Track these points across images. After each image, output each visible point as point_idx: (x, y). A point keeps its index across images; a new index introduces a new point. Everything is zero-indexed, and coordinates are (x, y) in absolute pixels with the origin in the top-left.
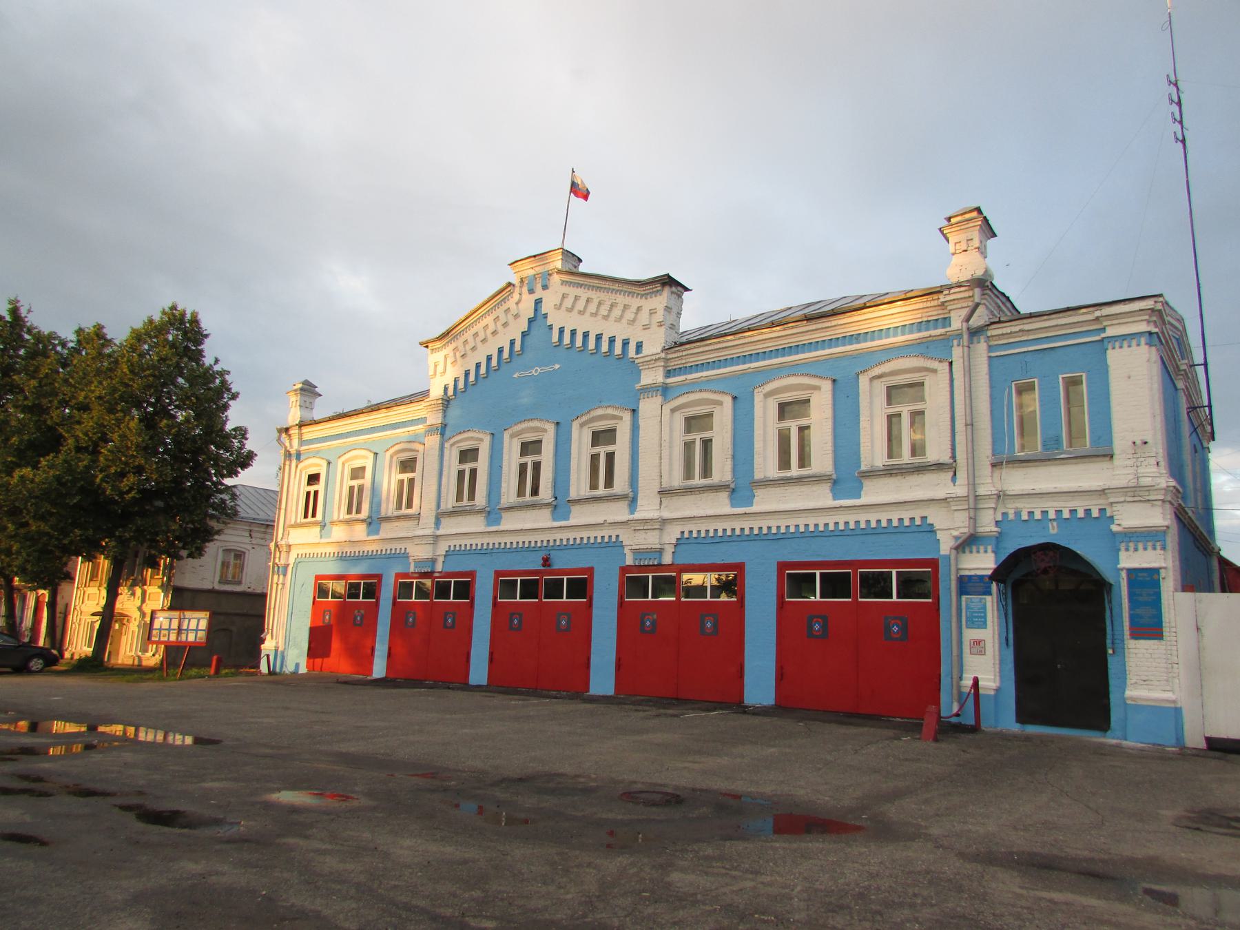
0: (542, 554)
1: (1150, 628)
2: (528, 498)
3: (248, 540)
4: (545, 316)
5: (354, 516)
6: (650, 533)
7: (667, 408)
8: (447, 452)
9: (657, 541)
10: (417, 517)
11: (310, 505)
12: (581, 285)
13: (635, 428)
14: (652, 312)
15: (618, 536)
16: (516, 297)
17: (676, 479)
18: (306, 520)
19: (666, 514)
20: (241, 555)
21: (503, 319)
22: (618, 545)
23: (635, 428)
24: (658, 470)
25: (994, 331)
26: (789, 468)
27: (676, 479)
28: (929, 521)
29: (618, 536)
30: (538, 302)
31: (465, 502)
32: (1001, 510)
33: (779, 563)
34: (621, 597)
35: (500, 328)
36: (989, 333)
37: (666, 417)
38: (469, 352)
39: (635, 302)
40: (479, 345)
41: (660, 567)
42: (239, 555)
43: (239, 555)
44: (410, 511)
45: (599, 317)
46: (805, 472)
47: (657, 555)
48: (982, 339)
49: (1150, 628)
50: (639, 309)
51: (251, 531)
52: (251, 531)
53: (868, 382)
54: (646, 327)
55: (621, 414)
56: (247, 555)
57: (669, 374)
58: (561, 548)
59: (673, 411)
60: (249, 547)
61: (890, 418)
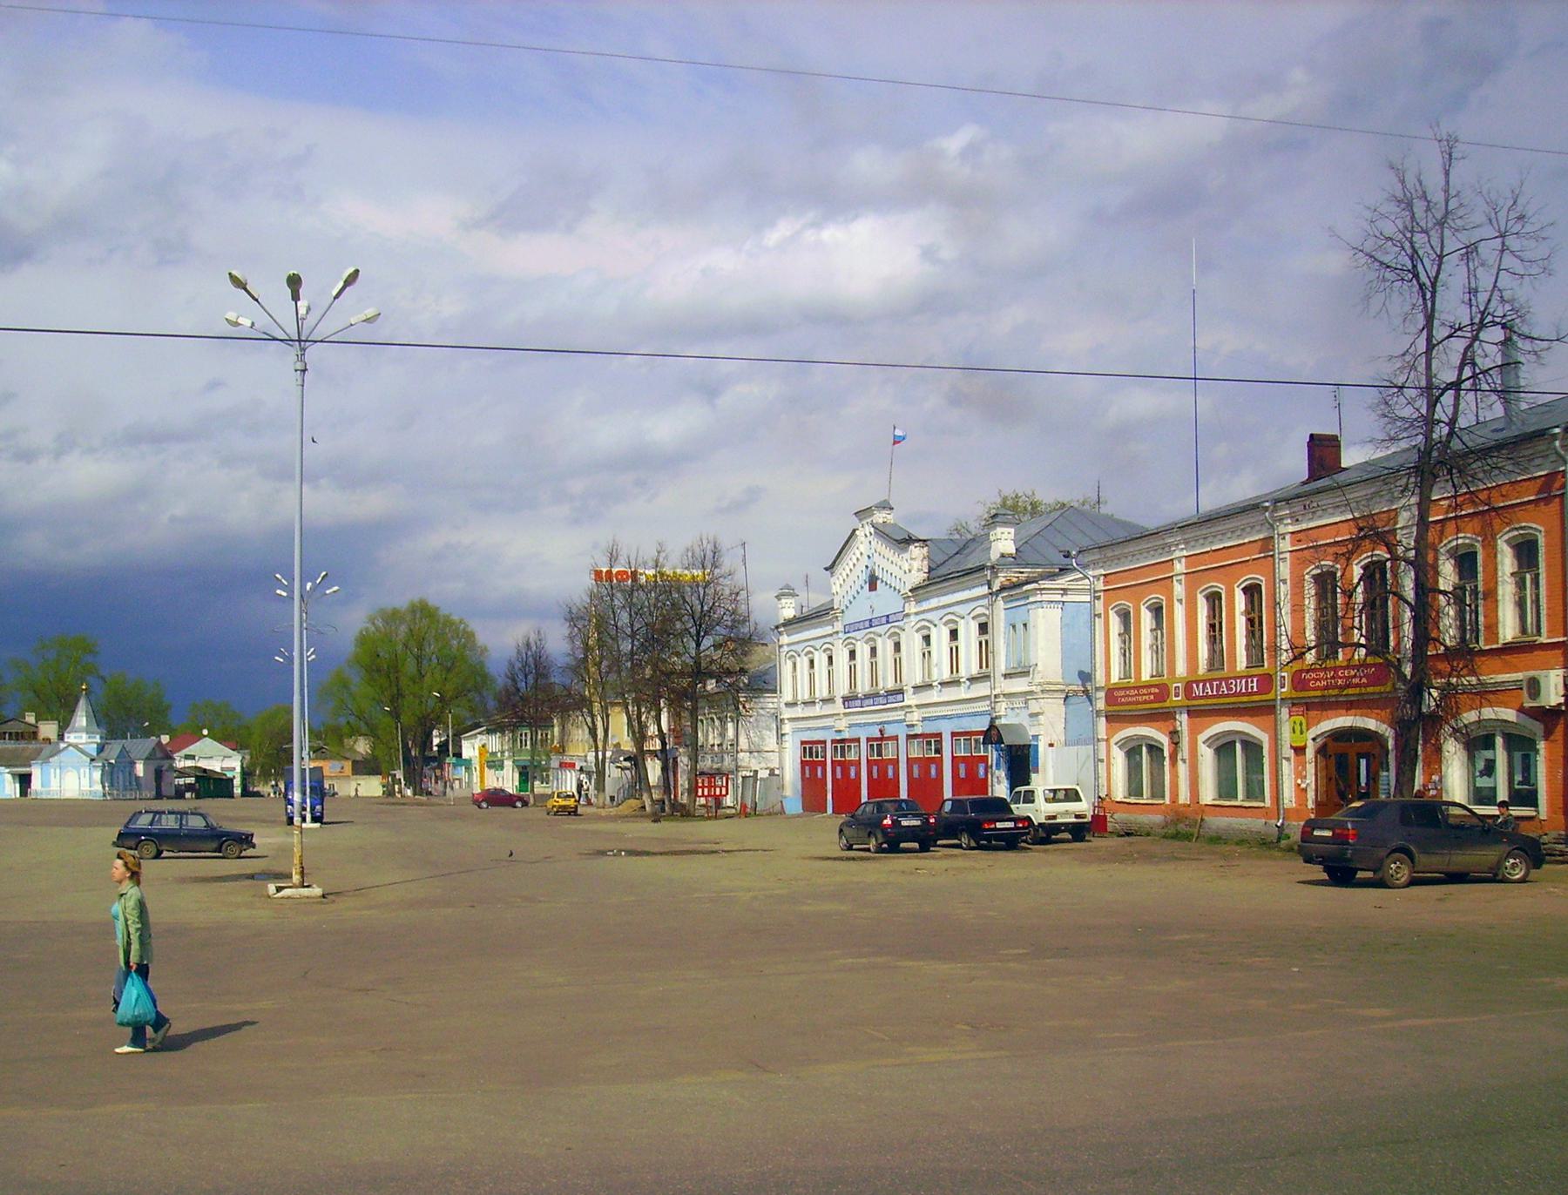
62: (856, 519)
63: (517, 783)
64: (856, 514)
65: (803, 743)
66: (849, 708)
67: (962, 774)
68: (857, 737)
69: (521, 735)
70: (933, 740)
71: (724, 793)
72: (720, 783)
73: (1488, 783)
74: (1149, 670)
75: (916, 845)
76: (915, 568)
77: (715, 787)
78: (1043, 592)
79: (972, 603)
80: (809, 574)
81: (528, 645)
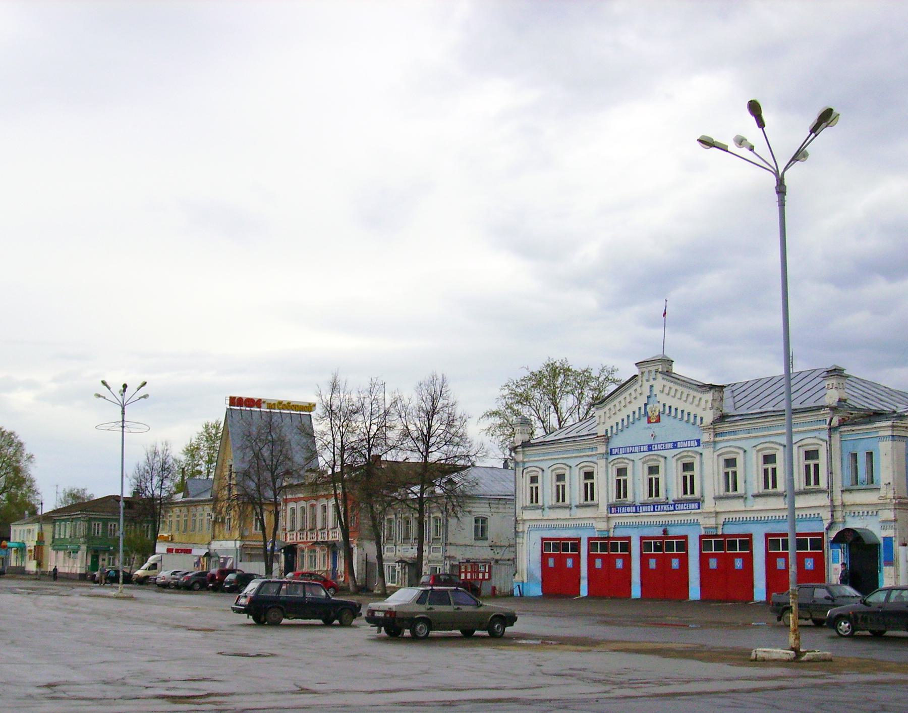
0: (663, 528)
1: (890, 562)
2: (812, 486)
3: (488, 510)
4: (656, 395)
5: (654, 498)
6: (712, 519)
7: (716, 454)
8: (610, 470)
9: (714, 523)
10: (597, 506)
11: (534, 496)
12: (672, 382)
13: (701, 463)
14: (706, 402)
15: (697, 520)
16: (640, 383)
17: (722, 491)
18: (767, 491)
19: (718, 510)
20: (485, 520)
21: (634, 395)
22: (698, 524)
23: (701, 463)
24: (712, 487)
25: (843, 429)
26: (687, 494)
27: (722, 491)
28: (820, 515)
29: (697, 520)
30: (651, 387)
31: (812, 486)
32: (845, 511)
33: (751, 535)
34: (701, 551)
35: (638, 395)
36: (840, 430)
37: (715, 457)
38: (633, 400)
39: (698, 395)
40: (633, 400)
41: (716, 536)
42: (484, 520)
43: (484, 520)
44: (592, 502)
45: (682, 400)
46: (735, 493)
47: (714, 530)
48: (838, 432)
49: (890, 562)
50: (700, 399)
51: (489, 503)
52: (489, 503)
53: (796, 449)
54: (704, 409)
55: (695, 456)
56: (489, 520)
57: (716, 435)
58: (672, 525)
59: (718, 456)
60: (490, 514)
61: (806, 466)
62: (636, 367)
63: (89, 564)
64: (636, 364)
65: (543, 539)
66: (617, 512)
67: (713, 564)
68: (579, 537)
69: (111, 525)
70: (738, 539)
71: (487, 577)
72: (483, 569)
73: (341, 563)
74: (840, 484)
75: (320, 622)
76: (715, 407)
77: (478, 573)
78: (896, 429)
79: (801, 434)
80: (147, 384)
81: (155, 454)
